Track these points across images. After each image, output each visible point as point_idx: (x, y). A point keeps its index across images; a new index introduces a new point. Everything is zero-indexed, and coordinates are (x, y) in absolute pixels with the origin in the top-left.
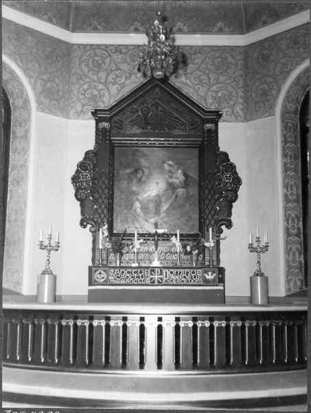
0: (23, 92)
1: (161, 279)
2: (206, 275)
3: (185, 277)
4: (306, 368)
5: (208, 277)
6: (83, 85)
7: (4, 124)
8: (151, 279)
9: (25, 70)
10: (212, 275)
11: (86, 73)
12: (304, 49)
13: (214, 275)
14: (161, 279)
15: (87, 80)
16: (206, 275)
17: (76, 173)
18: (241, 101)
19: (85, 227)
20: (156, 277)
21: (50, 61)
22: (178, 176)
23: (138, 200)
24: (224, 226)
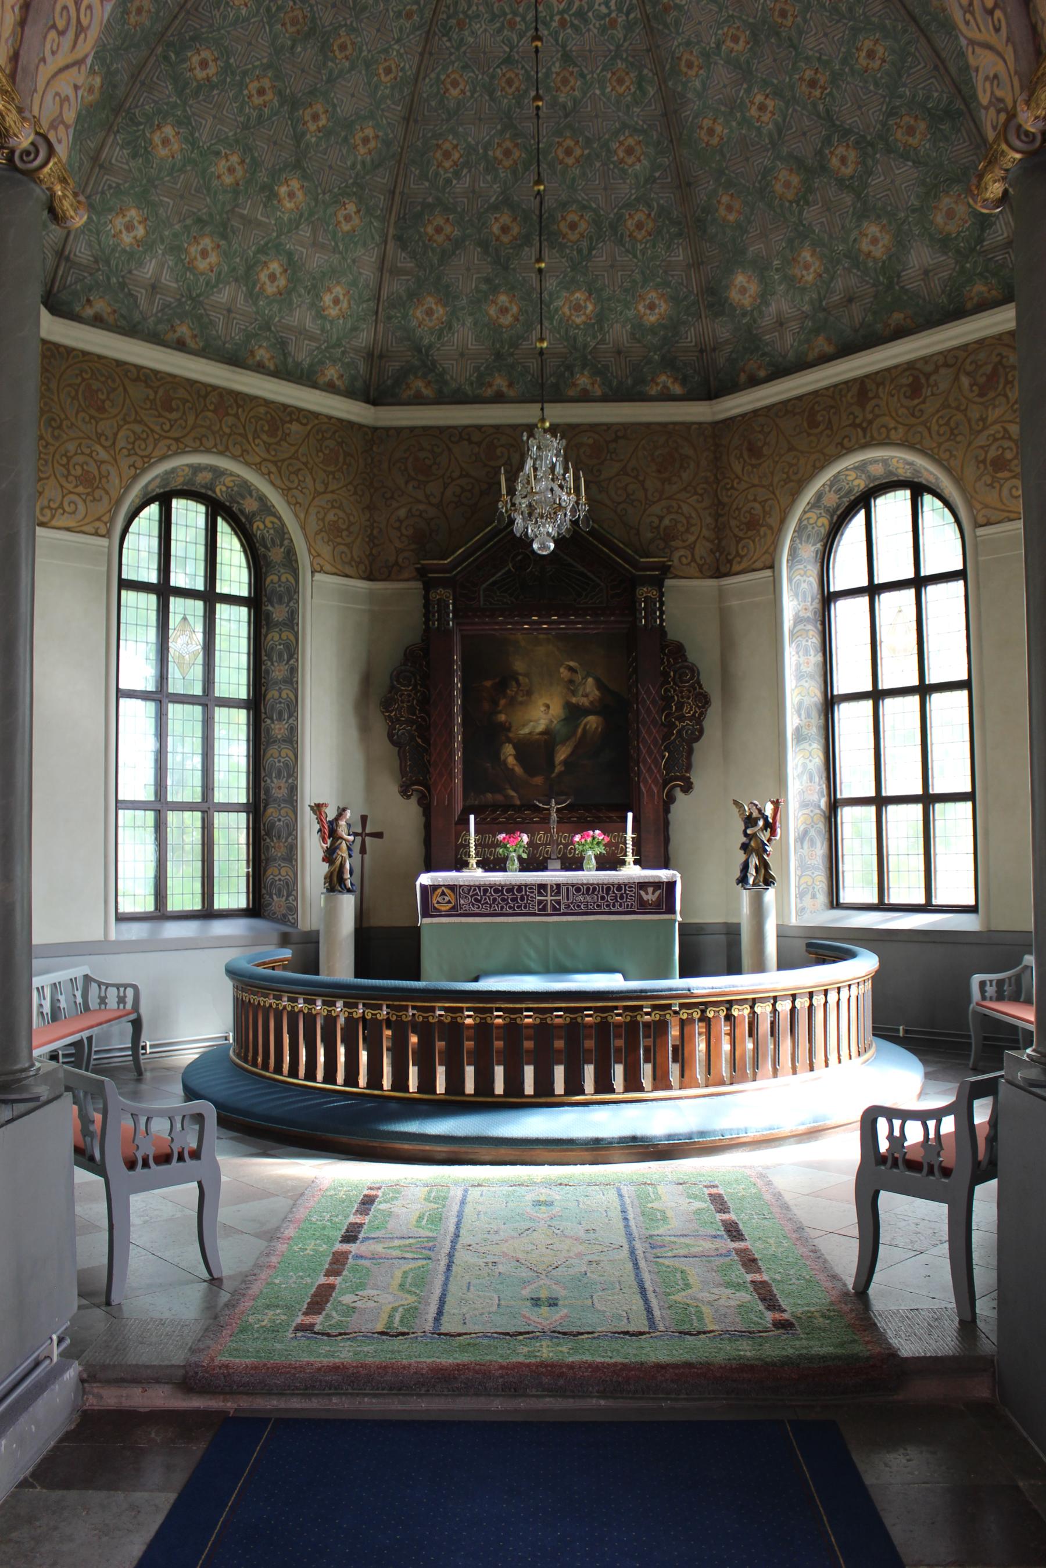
0: (249, 487)
1: (559, 903)
2: (642, 893)
3: (603, 898)
4: (356, 976)
5: (645, 897)
6: (398, 508)
8: (540, 902)
9: (285, 492)
12: (829, 436)
13: (658, 893)
16: (642, 893)
17: (390, 692)
19: (409, 797)
20: (549, 898)
21: (331, 468)
22: (588, 690)
23: (509, 740)
24: (678, 789)
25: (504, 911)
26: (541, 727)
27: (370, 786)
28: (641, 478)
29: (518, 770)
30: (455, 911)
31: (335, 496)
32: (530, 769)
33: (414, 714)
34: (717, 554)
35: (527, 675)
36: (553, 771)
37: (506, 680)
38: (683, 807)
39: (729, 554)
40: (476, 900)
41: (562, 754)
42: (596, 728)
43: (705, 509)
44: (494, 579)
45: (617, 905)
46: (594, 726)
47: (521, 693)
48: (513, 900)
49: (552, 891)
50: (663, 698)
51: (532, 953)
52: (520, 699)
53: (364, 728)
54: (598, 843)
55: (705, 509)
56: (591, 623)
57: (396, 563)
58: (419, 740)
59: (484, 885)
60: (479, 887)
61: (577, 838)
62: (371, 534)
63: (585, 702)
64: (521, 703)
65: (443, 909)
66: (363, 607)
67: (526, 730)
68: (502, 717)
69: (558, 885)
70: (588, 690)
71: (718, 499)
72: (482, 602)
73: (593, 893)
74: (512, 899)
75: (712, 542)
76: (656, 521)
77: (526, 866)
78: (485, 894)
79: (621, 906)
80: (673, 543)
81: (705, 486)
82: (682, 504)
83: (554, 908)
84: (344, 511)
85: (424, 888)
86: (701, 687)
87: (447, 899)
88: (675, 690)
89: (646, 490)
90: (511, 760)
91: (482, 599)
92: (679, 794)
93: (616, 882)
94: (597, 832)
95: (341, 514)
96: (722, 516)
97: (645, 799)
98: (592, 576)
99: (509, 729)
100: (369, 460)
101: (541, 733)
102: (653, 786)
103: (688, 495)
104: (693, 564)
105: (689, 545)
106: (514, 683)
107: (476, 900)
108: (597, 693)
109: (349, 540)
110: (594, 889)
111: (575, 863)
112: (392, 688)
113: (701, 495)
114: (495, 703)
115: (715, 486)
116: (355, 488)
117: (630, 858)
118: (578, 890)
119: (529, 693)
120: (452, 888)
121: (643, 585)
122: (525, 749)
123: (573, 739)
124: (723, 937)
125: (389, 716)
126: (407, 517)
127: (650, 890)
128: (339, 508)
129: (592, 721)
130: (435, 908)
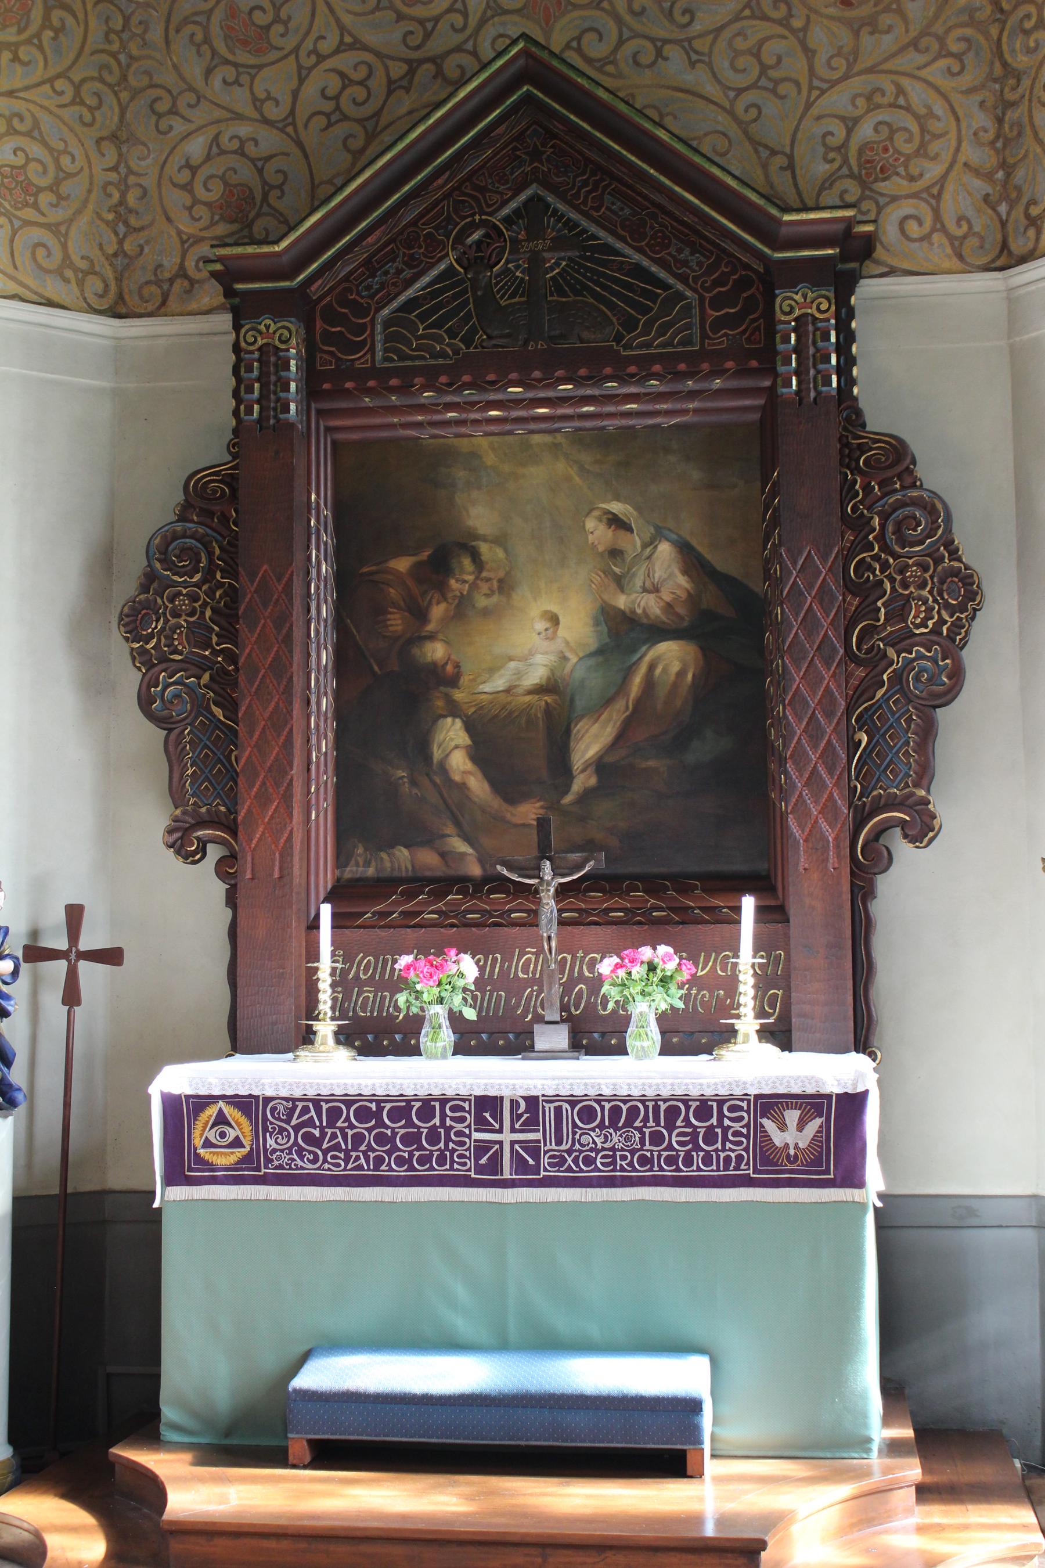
2: (769, 1125)
3: (657, 1138)
5: (778, 1138)
7: (855, 364)
8: (482, 1148)
10: (800, 1127)
11: (199, 83)
13: (814, 1126)
14: (534, 1150)
15: (200, 115)
16: (769, 1125)
17: (145, 588)
18: (970, 153)
20: (507, 1137)
22: (658, 574)
23: (454, 710)
24: (898, 831)
25: (383, 1171)
26: (536, 675)
27: (108, 830)
28: (797, 23)
29: (478, 786)
30: (251, 1170)
31: (18, 106)
32: (508, 785)
33: (207, 645)
34: (1003, 208)
35: (500, 540)
36: (567, 790)
37: (446, 555)
38: (911, 880)
39: (1033, 202)
40: (308, 1138)
41: (590, 743)
42: (681, 674)
43: (971, 91)
44: (410, 293)
45: (698, 1158)
46: (675, 667)
47: (484, 588)
48: (407, 1140)
49: (515, 1117)
50: (849, 587)
51: (461, 1292)
52: (482, 602)
53: (94, 686)
54: (664, 981)
55: (971, 91)
56: (662, 397)
57: (182, 273)
58: (218, 712)
59: (331, 1098)
60: (317, 1102)
61: (606, 967)
62: (122, 202)
63: (650, 606)
64: (486, 612)
65: (221, 1161)
66: (104, 384)
67: (498, 683)
68: (436, 651)
69: (532, 1102)
70: (658, 574)
71: (1005, 64)
72: (379, 355)
73: (629, 1123)
74: (407, 1140)
75: (989, 176)
76: (840, 132)
77: (471, 1040)
78: (331, 1124)
79: (707, 1161)
80: (882, 186)
81: (968, 32)
82: (905, 82)
83: (520, 1165)
84: (45, 144)
85: (172, 1105)
86: (954, 553)
87: (232, 1134)
88: (885, 566)
89: (810, 53)
90: (459, 763)
91: (379, 346)
92: (903, 850)
93: (695, 1093)
94: (663, 949)
95: (36, 150)
96: (1013, 104)
97: (801, 860)
98: (663, 274)
99: (453, 681)
100: (118, 23)
101: (540, 690)
102: (824, 826)
103: (921, 59)
104: (936, 237)
105: (927, 189)
106: (467, 562)
107: (308, 1138)
108: (682, 580)
109: (56, 216)
110: (633, 1112)
111: (597, 1033)
112: (149, 578)
113: (959, 57)
114: (421, 615)
115: (994, 31)
116: (77, 88)
117: (748, 1024)
118: (588, 1114)
119: (505, 586)
120: (246, 1104)
121: (792, 285)
122: (495, 737)
123: (620, 704)
124: (1030, 1234)
125: (142, 651)
126: (208, 158)
127: (792, 1116)
128: (28, 134)
129: (671, 657)
130: (199, 1160)
